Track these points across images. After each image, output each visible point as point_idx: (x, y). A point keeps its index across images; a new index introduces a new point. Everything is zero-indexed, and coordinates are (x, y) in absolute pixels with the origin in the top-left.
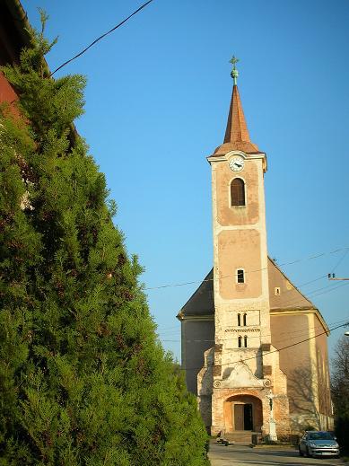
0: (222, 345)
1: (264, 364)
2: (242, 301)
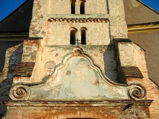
1: (124, 62)
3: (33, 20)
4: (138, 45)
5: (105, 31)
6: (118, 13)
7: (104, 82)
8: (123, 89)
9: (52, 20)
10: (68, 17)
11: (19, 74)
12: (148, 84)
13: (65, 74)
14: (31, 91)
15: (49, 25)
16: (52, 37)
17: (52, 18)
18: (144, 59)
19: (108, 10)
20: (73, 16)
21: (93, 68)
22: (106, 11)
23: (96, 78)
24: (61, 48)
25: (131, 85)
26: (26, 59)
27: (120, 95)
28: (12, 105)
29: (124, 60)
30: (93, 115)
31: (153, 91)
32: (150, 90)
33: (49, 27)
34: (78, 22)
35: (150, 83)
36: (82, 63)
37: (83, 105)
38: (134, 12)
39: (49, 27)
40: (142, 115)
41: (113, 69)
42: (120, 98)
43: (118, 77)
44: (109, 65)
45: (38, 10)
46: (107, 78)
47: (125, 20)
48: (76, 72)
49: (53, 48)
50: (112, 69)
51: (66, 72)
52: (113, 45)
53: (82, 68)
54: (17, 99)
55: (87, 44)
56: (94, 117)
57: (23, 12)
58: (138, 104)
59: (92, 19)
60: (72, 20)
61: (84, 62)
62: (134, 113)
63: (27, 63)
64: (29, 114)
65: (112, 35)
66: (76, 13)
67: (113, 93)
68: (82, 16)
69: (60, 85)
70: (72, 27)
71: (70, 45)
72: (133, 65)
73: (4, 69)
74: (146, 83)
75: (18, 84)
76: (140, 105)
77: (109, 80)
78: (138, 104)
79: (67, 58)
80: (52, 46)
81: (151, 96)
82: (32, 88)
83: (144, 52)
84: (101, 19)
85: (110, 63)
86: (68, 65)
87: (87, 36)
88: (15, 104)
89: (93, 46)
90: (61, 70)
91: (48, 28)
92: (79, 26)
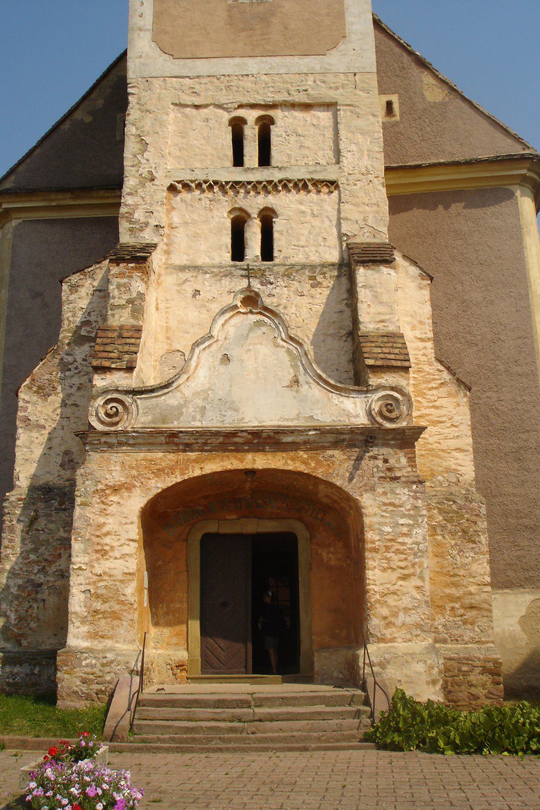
0: (149, 248)
1: (368, 321)
2: (253, 65)
3: (126, 189)
4: (415, 263)
5: (326, 219)
6: (366, 162)
7: (311, 381)
8: (357, 400)
9: (179, 186)
10: (223, 177)
11: (106, 364)
12: (431, 371)
13: (217, 362)
14: (137, 406)
15: (173, 202)
16: (181, 238)
17: (179, 182)
18: (429, 303)
19: (338, 153)
20: (238, 175)
21: (285, 344)
22: (331, 154)
23: (291, 371)
24: (206, 273)
25: (380, 387)
26: (120, 318)
27: (349, 415)
28: (96, 442)
29: (368, 313)
30: (283, 462)
31: (443, 391)
32: (435, 388)
33: (173, 208)
34: (252, 193)
35: (438, 370)
36: (259, 332)
37: (261, 440)
38: (427, 120)
39: (173, 208)
40: (398, 461)
41: (344, 332)
42: (347, 421)
43: (353, 355)
44: (334, 322)
45: (139, 157)
46: (319, 372)
47: (382, 184)
48: (245, 357)
49: (187, 275)
50: (339, 333)
51: (220, 356)
52: (347, 264)
53: (258, 347)
54: (106, 429)
55: (276, 261)
56: (286, 468)
57: (88, 119)
58: (390, 437)
59: (289, 181)
60: (235, 185)
61: (264, 329)
62: (379, 457)
63: (121, 328)
64: (136, 460)
65: (345, 232)
66: (246, 159)
67: (332, 408)
68: (264, 175)
69: (205, 391)
70: (236, 206)
71: (233, 263)
72: (391, 328)
73: (61, 336)
74: (427, 370)
75: (106, 391)
76: (393, 439)
77: (324, 376)
78: (390, 437)
79: (221, 321)
80: (183, 268)
81: (437, 404)
82: (142, 402)
83: (429, 282)
84: (316, 183)
85: (336, 315)
86: (225, 338)
87: (276, 235)
88: (103, 440)
89: (292, 266)
90: (207, 351)
91: (169, 212)
92: (254, 203)
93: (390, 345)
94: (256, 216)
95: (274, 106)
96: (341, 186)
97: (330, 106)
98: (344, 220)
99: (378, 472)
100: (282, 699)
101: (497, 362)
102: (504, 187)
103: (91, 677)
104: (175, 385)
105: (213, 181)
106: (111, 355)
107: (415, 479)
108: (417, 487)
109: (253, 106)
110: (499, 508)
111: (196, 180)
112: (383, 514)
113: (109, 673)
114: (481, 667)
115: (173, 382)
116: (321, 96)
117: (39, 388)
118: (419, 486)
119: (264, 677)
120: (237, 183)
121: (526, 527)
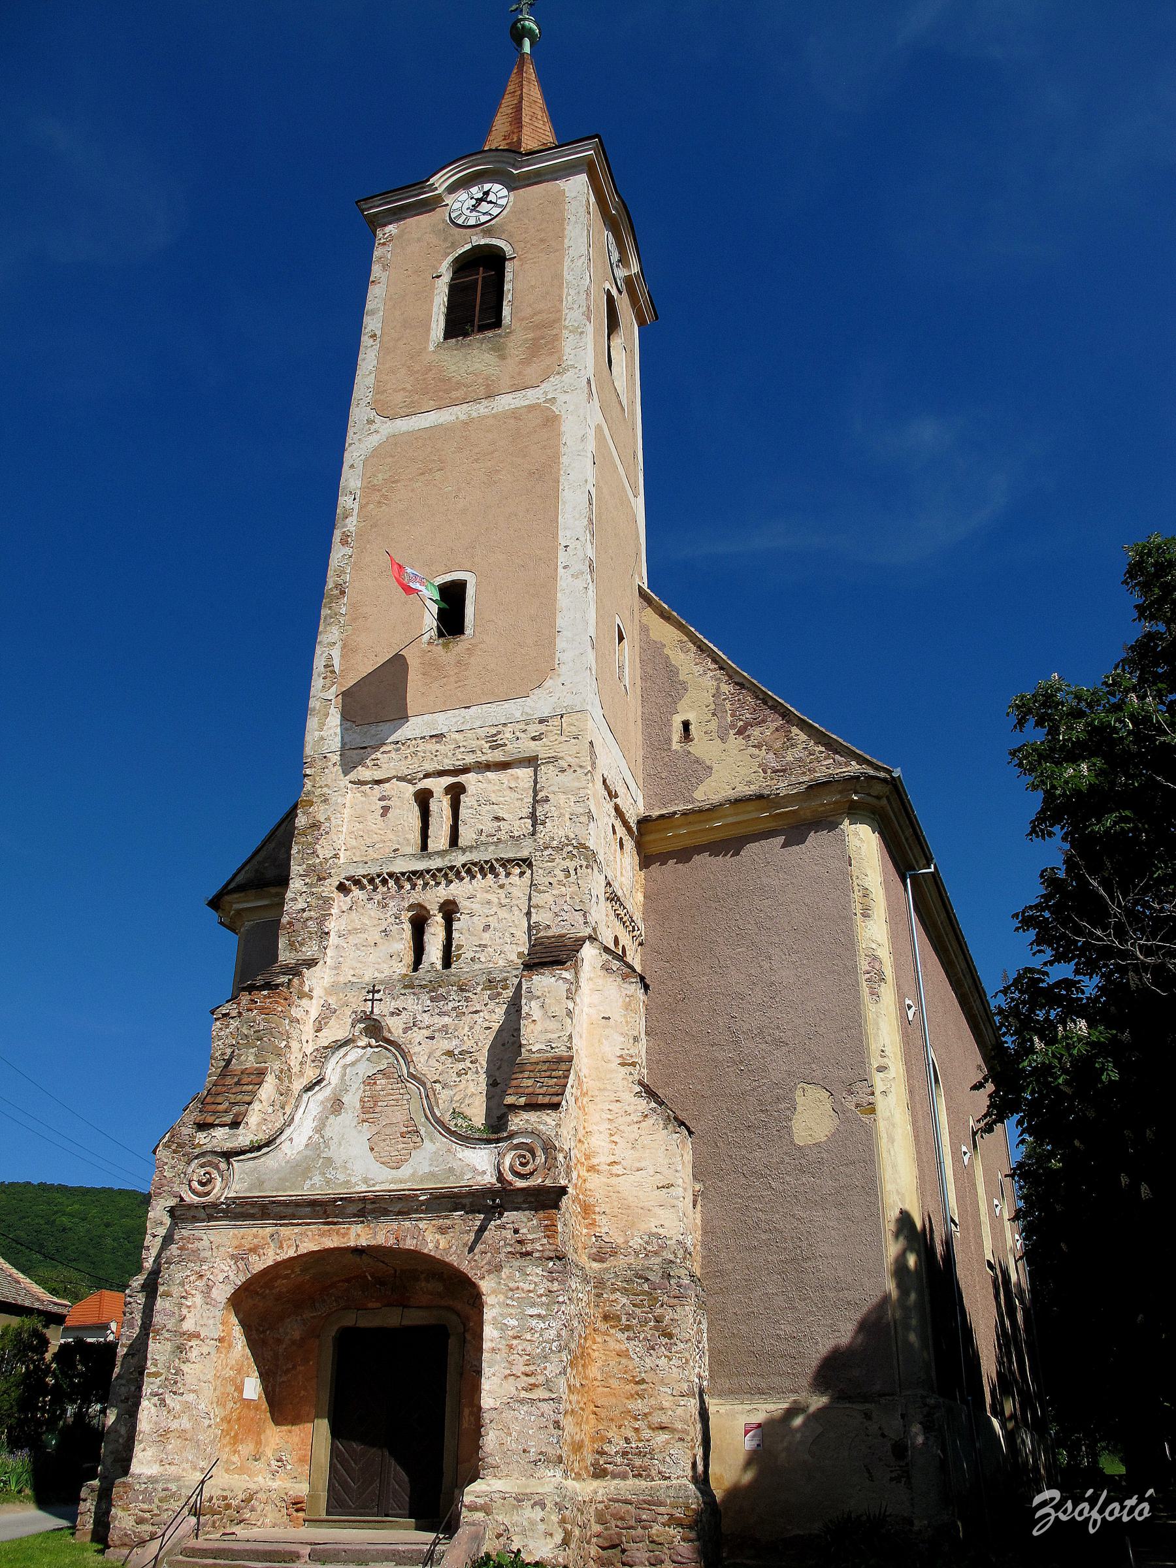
93: (548, 1073)
94: (436, 912)
95: (465, 770)
96: (534, 863)
97: (532, 761)
98: (535, 907)
99: (506, 1245)
100: (345, 1551)
101: (813, 1066)
102: (829, 819)
103: (147, 1515)
104: (278, 1141)
105: (387, 874)
106: (221, 1107)
107: (552, 1254)
108: (554, 1264)
109: (441, 773)
110: (811, 1276)
111: (369, 874)
112: (509, 1302)
113: (167, 1510)
114: (667, 1514)
115: (275, 1139)
116: (520, 750)
117: (179, 1145)
118: (558, 1263)
119: (383, 1522)
120: (414, 873)
121: (849, 1303)
